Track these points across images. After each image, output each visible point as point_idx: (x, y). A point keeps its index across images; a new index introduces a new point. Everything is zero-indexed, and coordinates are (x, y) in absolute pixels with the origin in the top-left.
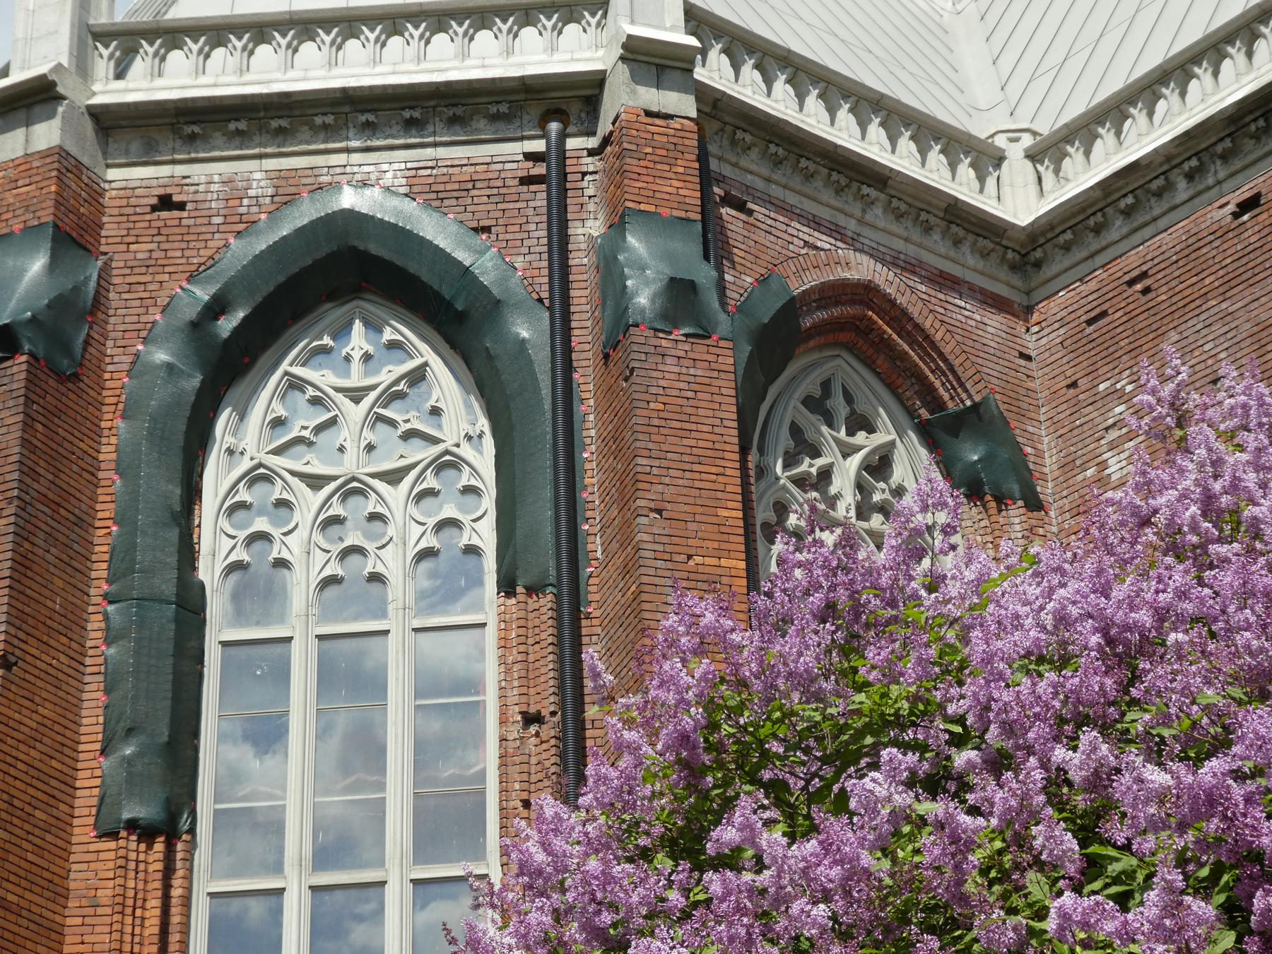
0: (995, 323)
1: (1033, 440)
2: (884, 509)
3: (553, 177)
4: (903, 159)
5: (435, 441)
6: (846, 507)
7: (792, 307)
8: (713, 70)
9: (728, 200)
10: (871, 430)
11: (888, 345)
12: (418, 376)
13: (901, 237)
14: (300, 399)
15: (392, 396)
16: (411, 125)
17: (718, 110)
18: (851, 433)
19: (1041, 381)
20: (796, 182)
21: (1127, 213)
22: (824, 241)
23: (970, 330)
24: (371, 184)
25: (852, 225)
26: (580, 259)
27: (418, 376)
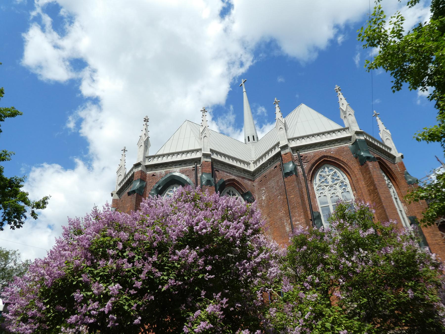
3: (196, 169)
4: (238, 165)
7: (224, 182)
8: (214, 156)
9: (216, 170)
10: (235, 195)
11: (237, 186)
13: (238, 173)
16: (180, 165)
17: (214, 161)
19: (256, 189)
20: (225, 168)
21: (263, 169)
22: (228, 174)
24: (177, 172)
26: (199, 178)
27: (335, 172)
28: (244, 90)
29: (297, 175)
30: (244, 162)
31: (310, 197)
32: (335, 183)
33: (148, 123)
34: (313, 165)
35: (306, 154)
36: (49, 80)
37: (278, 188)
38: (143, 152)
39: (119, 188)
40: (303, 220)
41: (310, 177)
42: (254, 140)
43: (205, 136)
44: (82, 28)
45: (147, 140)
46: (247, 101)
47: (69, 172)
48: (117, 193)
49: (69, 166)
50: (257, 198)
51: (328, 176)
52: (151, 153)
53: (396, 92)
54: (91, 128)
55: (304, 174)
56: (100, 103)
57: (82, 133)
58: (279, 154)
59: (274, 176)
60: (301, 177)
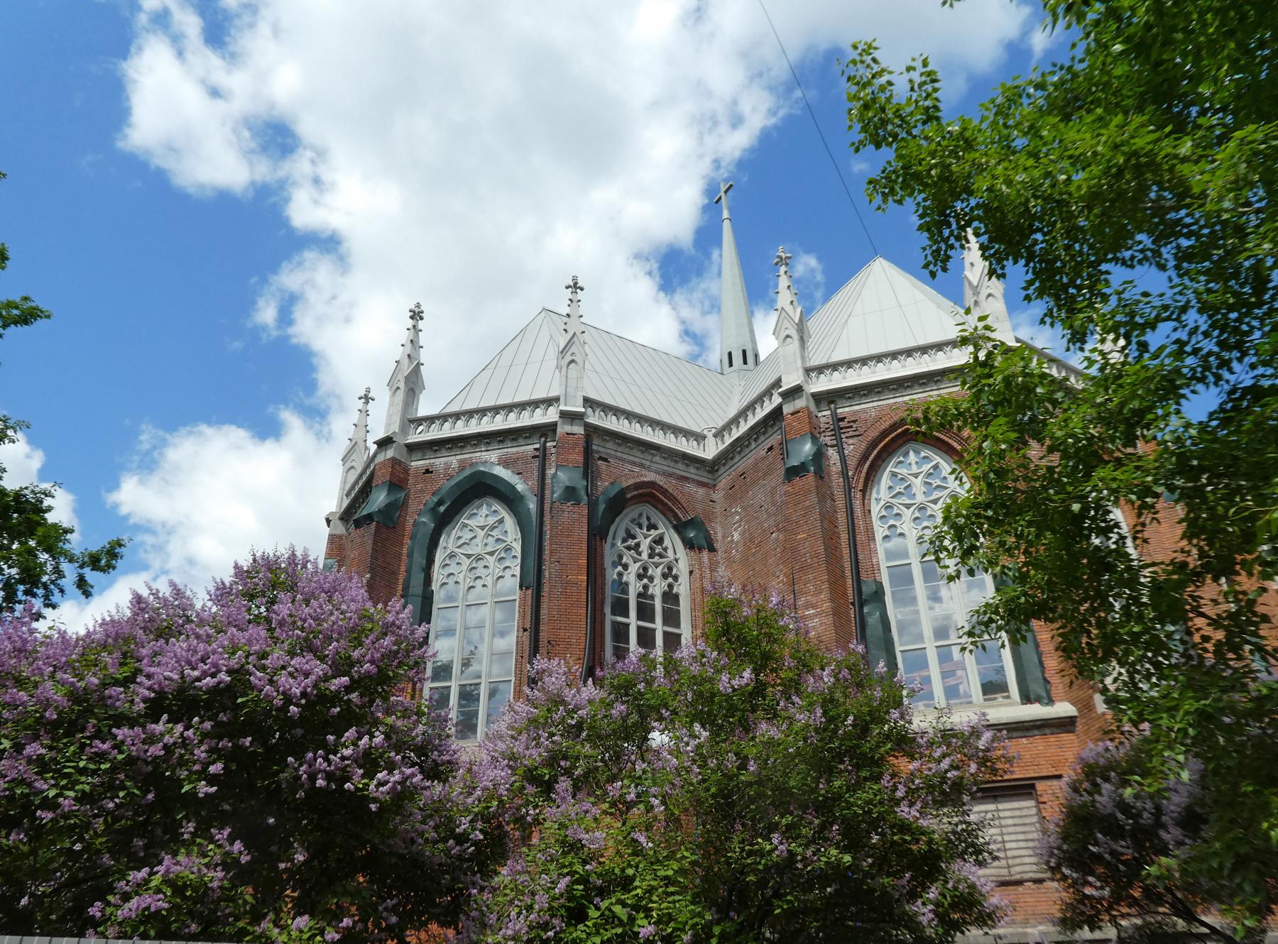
0: (701, 491)
1: (713, 529)
2: (661, 556)
3: (542, 456)
6: (645, 556)
7: (623, 492)
8: (594, 419)
9: (600, 458)
10: (656, 528)
11: (661, 501)
12: (501, 521)
14: (466, 530)
15: (493, 528)
17: (593, 432)
18: (648, 530)
19: (718, 509)
20: (627, 450)
21: (740, 453)
23: (693, 495)
24: (491, 460)
25: (648, 463)
26: (548, 481)
27: (936, 467)
28: (726, 214)
29: (821, 474)
30: (687, 434)
31: (858, 538)
32: (933, 497)
33: (421, 324)
34: (873, 445)
35: (855, 412)
36: (202, 186)
37: (772, 509)
39: (346, 502)
40: (827, 605)
41: (862, 480)
42: (745, 363)
43: (573, 361)
44: (276, 31)
45: (416, 371)
46: (733, 246)
47: (270, 445)
48: (341, 519)
49: (267, 430)
50: (719, 536)
51: (916, 475)
52: (424, 410)
53: (940, 273)
54: (321, 320)
55: (844, 473)
56: (343, 249)
57: (295, 336)
58: (777, 414)
59: (765, 474)
60: (837, 481)
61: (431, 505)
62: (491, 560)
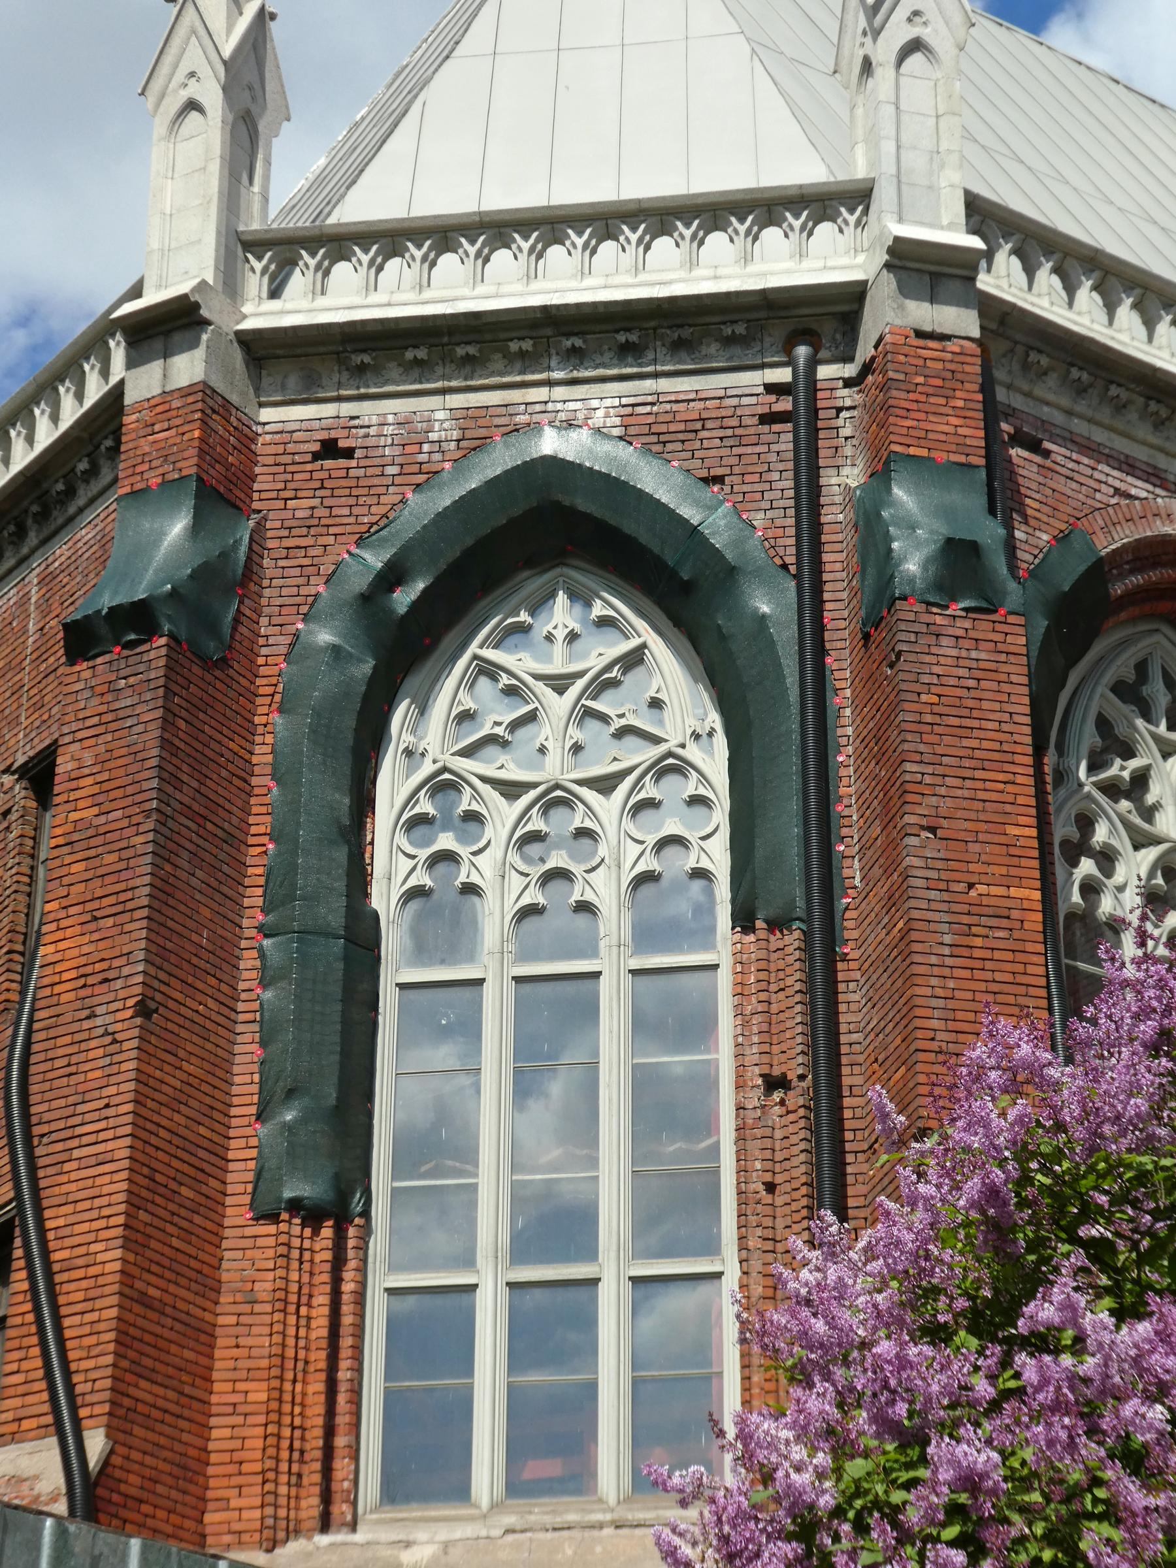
5: (656, 740)
7: (1100, 571)
8: (1003, 279)
9: (1018, 439)
15: (602, 685)
16: (628, 351)
22: (1139, 488)
24: (579, 424)
27: (634, 659)
38: (213, 180)
61: (360, 582)
62: (607, 810)
